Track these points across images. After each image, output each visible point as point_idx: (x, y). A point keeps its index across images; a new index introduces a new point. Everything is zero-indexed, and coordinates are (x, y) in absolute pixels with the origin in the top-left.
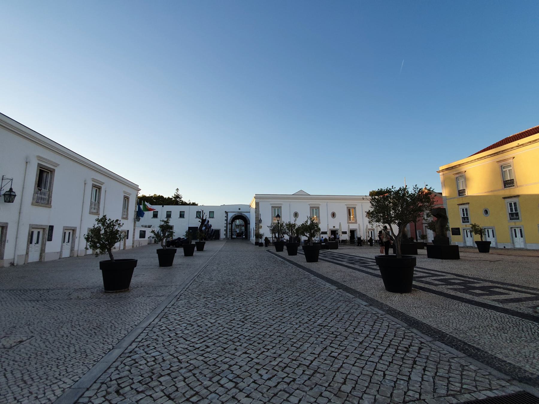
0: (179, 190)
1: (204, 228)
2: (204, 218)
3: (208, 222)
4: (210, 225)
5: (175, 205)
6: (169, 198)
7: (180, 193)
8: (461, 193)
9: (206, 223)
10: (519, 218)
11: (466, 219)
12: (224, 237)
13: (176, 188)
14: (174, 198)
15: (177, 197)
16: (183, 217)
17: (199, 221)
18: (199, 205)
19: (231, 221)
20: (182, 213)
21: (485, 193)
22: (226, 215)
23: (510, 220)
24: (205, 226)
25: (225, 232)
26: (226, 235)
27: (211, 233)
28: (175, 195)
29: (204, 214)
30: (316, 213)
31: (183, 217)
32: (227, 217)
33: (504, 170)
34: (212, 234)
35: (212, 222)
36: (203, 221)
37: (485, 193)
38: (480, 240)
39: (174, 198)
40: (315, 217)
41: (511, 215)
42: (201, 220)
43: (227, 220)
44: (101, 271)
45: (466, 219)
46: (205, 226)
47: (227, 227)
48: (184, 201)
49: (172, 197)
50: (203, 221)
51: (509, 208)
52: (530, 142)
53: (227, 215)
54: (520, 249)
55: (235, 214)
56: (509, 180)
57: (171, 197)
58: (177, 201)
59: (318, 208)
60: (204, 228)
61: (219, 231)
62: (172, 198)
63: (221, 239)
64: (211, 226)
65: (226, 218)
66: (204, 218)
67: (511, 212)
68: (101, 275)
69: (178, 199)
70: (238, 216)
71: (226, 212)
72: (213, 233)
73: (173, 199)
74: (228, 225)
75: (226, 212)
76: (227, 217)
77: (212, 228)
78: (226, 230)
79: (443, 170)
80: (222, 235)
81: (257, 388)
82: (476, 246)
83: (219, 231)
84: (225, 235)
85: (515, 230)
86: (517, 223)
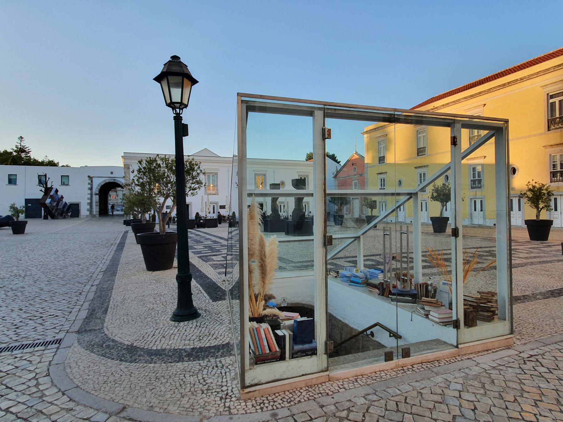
0: (25, 139)
1: (48, 201)
2: (49, 186)
3: (57, 191)
4: (60, 196)
5: (10, 164)
6: (6, 152)
7: (26, 144)
8: (382, 159)
9: (52, 193)
10: (481, 186)
11: (477, 182)
12: (88, 213)
13: (19, 136)
14: (15, 151)
15: (22, 150)
16: (15, 183)
17: (41, 191)
18: (60, 165)
19: (98, 190)
20: (13, 177)
21: (404, 160)
22: (90, 181)
23: (471, 188)
24: (52, 197)
25: (88, 207)
26: (91, 210)
27: (64, 207)
28: (16, 147)
29: (47, 179)
30: (213, 180)
31: (15, 183)
32: (91, 183)
33: (419, 136)
34: (65, 209)
35: (63, 191)
36: (48, 190)
37: (401, 161)
38: (370, 214)
39: (15, 151)
40: (212, 185)
41: (474, 182)
42: (43, 189)
43: (91, 189)
44: (139, 246)
45: (477, 182)
46: (52, 197)
47: (91, 199)
48: (32, 157)
49: (12, 151)
50: (48, 190)
51: (472, 173)
52: (443, 105)
53: (92, 181)
54: (480, 226)
55: (105, 181)
56: (421, 148)
57: (9, 150)
58: (21, 158)
59: (216, 174)
60: (48, 201)
61: (78, 204)
62: (11, 153)
63: (82, 217)
64: (62, 197)
65: (90, 186)
66: (49, 186)
67: (561, 169)
68: (141, 251)
69: (23, 155)
70: (109, 183)
71: (89, 176)
72: (66, 207)
73: (15, 154)
74: (94, 196)
75: (89, 176)
76: (91, 183)
77: (64, 200)
78: (91, 204)
79: (367, 132)
80: (84, 210)
81: (511, 418)
82: (431, 222)
83: (78, 204)
84: (88, 210)
85: (475, 201)
86: (478, 192)
